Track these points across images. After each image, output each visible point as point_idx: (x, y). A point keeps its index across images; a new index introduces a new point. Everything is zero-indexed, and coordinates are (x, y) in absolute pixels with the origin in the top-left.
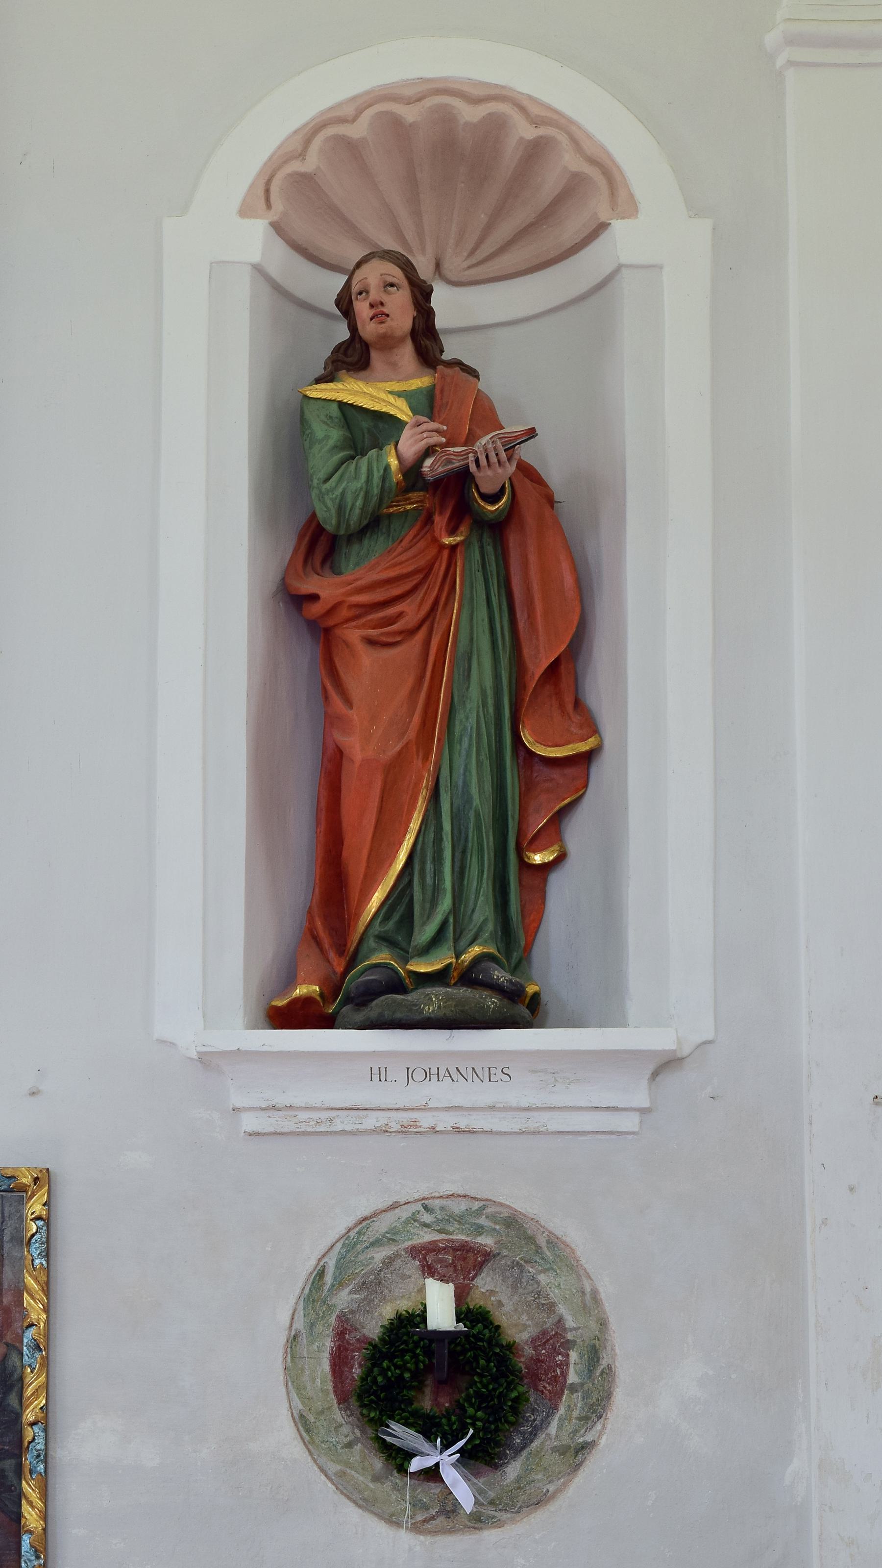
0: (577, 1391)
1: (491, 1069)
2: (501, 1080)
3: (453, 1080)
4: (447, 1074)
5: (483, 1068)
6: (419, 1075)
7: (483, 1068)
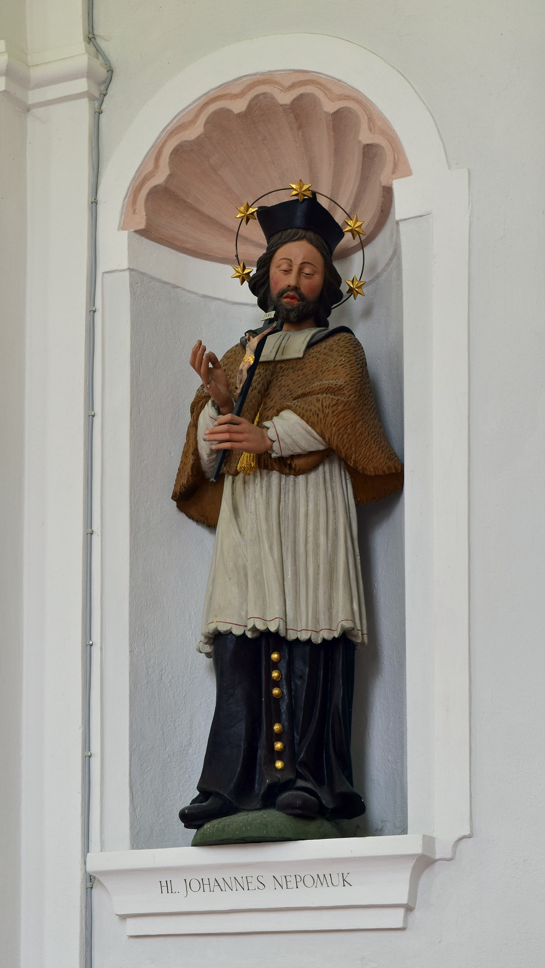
0: (348, 292)
1: (296, 876)
2: (258, 888)
3: (222, 890)
4: (216, 884)
5: (230, 878)
6: (195, 885)
7: (230, 878)
